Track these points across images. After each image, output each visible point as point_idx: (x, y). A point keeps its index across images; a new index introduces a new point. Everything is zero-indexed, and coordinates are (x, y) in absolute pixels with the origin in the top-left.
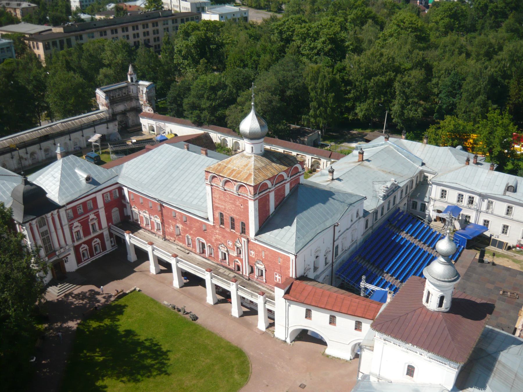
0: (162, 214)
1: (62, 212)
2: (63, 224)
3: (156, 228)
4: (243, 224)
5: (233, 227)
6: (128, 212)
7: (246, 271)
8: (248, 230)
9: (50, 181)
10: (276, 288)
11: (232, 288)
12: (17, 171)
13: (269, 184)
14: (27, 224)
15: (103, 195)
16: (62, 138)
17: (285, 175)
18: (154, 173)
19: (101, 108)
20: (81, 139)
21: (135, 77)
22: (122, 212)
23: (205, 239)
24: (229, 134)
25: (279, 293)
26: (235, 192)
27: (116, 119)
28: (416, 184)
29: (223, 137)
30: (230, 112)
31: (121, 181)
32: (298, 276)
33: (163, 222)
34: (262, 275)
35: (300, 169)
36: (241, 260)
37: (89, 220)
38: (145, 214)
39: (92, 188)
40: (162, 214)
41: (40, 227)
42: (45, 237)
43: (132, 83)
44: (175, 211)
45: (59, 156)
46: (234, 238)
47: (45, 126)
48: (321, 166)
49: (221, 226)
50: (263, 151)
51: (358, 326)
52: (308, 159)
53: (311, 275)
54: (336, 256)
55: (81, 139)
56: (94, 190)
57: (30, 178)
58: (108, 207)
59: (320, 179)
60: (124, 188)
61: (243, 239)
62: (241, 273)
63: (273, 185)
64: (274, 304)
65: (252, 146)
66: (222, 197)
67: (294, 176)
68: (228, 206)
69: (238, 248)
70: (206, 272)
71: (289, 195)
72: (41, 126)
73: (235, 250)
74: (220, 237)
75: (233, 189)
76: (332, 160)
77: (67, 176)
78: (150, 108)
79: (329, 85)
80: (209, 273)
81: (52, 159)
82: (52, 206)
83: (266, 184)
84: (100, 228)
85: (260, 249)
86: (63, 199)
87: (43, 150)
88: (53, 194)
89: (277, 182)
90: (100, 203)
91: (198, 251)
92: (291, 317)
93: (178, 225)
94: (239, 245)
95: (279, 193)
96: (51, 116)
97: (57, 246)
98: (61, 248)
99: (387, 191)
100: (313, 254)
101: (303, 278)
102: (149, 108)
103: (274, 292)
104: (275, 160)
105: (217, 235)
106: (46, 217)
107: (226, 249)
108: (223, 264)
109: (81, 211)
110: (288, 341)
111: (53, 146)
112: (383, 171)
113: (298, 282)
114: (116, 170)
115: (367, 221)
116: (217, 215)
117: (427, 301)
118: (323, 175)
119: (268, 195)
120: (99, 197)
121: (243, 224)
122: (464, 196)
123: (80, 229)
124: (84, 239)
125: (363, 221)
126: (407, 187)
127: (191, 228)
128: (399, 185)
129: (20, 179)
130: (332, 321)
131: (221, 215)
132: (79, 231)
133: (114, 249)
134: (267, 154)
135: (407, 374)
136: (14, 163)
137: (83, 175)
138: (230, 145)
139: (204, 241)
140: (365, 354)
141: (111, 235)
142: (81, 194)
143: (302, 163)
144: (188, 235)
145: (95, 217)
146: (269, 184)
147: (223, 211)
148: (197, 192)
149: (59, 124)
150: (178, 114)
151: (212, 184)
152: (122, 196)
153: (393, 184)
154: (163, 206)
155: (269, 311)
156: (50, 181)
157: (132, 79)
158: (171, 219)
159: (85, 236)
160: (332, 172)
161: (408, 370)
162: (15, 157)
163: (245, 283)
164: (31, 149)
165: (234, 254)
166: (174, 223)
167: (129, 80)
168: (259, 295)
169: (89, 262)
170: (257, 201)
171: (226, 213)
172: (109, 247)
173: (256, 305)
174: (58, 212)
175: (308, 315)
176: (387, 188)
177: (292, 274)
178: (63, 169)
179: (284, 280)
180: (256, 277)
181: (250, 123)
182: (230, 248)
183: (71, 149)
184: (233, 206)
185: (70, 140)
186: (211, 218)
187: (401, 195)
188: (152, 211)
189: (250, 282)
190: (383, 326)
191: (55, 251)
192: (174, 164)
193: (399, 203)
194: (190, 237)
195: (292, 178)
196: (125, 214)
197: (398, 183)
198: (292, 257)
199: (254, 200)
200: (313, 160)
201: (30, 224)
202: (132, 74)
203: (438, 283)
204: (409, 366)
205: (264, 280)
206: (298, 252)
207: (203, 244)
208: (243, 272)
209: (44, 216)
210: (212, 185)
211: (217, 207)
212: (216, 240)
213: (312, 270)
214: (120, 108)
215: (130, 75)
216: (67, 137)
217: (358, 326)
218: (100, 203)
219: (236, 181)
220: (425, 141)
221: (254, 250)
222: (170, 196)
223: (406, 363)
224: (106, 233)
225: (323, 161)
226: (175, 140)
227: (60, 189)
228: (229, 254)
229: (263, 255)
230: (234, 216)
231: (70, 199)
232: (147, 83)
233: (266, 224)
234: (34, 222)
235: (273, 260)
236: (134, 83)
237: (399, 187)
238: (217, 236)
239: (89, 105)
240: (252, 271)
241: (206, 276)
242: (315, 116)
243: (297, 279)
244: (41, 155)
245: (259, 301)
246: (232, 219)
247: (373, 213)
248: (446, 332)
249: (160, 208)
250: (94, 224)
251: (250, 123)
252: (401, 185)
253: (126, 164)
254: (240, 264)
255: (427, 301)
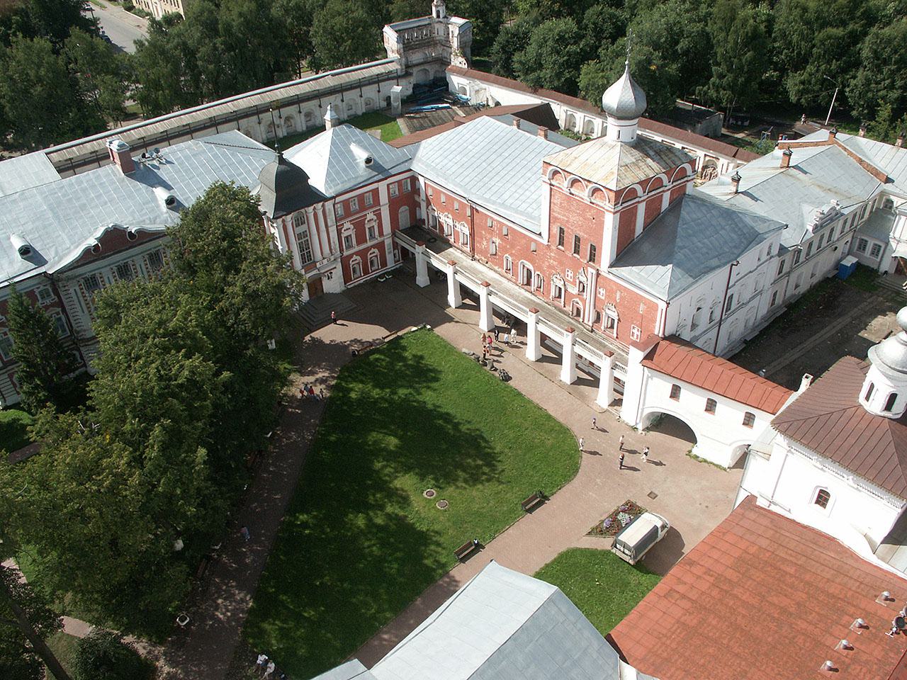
0: (472, 221)
1: (329, 205)
2: (329, 224)
3: (461, 241)
4: (593, 248)
5: (577, 251)
6: (423, 213)
7: (589, 317)
8: (600, 257)
9: (313, 158)
10: (631, 347)
11: (564, 340)
12: (269, 143)
13: (639, 189)
14: (280, 221)
15: (388, 185)
16: (332, 98)
17: (665, 178)
18: (465, 159)
19: (392, 55)
20: (358, 100)
21: (442, 10)
22: (413, 213)
23: (533, 264)
24: (580, 107)
25: (636, 355)
26: (586, 198)
27: (411, 74)
28: (871, 212)
29: (571, 111)
30: (587, 73)
31: (417, 167)
32: (666, 335)
33: (472, 234)
34: (612, 327)
35: (689, 172)
36: (584, 301)
37: (366, 222)
38: (446, 219)
39: (373, 175)
40: (472, 221)
41: (298, 225)
42: (303, 240)
43: (438, 19)
44: (491, 218)
45: (328, 125)
46: (576, 267)
47: (306, 82)
48: (719, 170)
49: (560, 247)
50: (635, 138)
51: (749, 420)
52: (699, 154)
53: (686, 336)
54: (726, 311)
55: (358, 100)
56: (376, 179)
57: (287, 154)
58: (394, 204)
59: (717, 189)
60: (420, 177)
61: (590, 270)
62: (581, 320)
63: (644, 192)
64: (626, 372)
65: (618, 129)
66: (565, 204)
67: (679, 182)
68: (574, 218)
69: (580, 282)
70: (530, 313)
71: (670, 210)
72: (300, 78)
73: (575, 285)
74: (555, 263)
75: (583, 193)
76: (739, 162)
77: (339, 154)
78: (463, 60)
79: (750, 35)
80: (534, 315)
81: (322, 128)
82: (314, 197)
83: (634, 191)
84: (381, 234)
85: (614, 287)
86: (331, 188)
87: (302, 115)
88: (318, 181)
89: (651, 190)
90: (384, 198)
91: (520, 281)
92: (647, 393)
93: (494, 239)
94: (583, 279)
95: (653, 205)
96: (316, 66)
97: (318, 256)
98: (324, 258)
99: (821, 219)
100: (693, 304)
101: (674, 338)
102: (461, 59)
103: (627, 353)
104: (652, 153)
105: (551, 259)
106: (306, 212)
107: (562, 282)
108: (556, 303)
109: (354, 207)
110: (640, 427)
111: (318, 108)
112: (819, 186)
113: (665, 343)
114: (410, 151)
115: (783, 263)
116: (556, 230)
117: (867, 398)
118: (723, 184)
119: (636, 208)
120: (382, 187)
121: (593, 248)
122: (869, 243)
123: (352, 232)
124: (357, 249)
125: (775, 263)
126: (855, 215)
127: (513, 246)
128: (842, 211)
129: (273, 155)
130: (711, 406)
131: (562, 231)
132: (350, 235)
133: (398, 266)
134: (641, 145)
135: (816, 503)
136: (262, 130)
137: (361, 154)
138: (579, 128)
139: (531, 268)
140: (754, 463)
141: (395, 245)
142: (355, 183)
143: (693, 162)
144: (507, 255)
145: (375, 218)
146: (639, 189)
147: (565, 226)
148: (528, 193)
149: (329, 79)
150: (507, 73)
151: (553, 182)
152: (415, 190)
153: (833, 209)
154: (477, 210)
155: (617, 380)
156: (313, 158)
157: (438, 12)
158: (485, 230)
159: (359, 243)
160: (737, 180)
161: (819, 496)
162: (263, 122)
163: (587, 337)
164: (306, 106)
165: (574, 290)
166: (489, 236)
167: (434, 14)
168: (604, 356)
169: (362, 281)
170: (619, 214)
171: (569, 228)
172: (391, 264)
173: (599, 369)
174: (323, 206)
175: (675, 393)
176: (823, 214)
177: (658, 330)
178: (333, 143)
179: (645, 337)
180: (603, 328)
181: (619, 93)
182: (569, 281)
183: (344, 116)
184: (581, 218)
185: (342, 101)
186: (545, 235)
187: (844, 227)
188: (458, 216)
189: (592, 334)
190: (790, 426)
191: (315, 262)
192: (496, 147)
193: (838, 240)
194: (510, 259)
195: (674, 184)
196: (418, 217)
197: (842, 208)
198: (662, 305)
199: (614, 213)
200: (707, 158)
201: (283, 221)
202: (439, 6)
203: (891, 373)
204: (821, 491)
205: (615, 335)
206: (672, 298)
207: (529, 272)
208: (583, 319)
209: (303, 210)
210: (551, 185)
211: (556, 218)
212: (550, 267)
213: (689, 327)
214: (416, 57)
215: (436, 6)
216: (339, 96)
217: (749, 420)
218: (384, 198)
219: (589, 181)
220: (899, 142)
221: (604, 288)
222: (487, 196)
223: (817, 487)
224: (388, 242)
225: (723, 161)
226: (497, 110)
227: (328, 174)
228: (566, 291)
229: (618, 297)
230: (581, 234)
231: (340, 188)
232: (461, 21)
233: (627, 253)
234: (289, 217)
235: (630, 304)
236: (441, 19)
237: (842, 214)
238: (552, 261)
239: (375, 51)
240: (598, 319)
241: (529, 319)
242: (717, 88)
243: (665, 338)
244: (300, 124)
245: (604, 364)
246: (577, 239)
247: (795, 251)
248: (892, 449)
249: (473, 214)
250: (373, 227)
251: (619, 93)
252: (846, 212)
253: (424, 143)
254: (581, 307)
255: (867, 398)
